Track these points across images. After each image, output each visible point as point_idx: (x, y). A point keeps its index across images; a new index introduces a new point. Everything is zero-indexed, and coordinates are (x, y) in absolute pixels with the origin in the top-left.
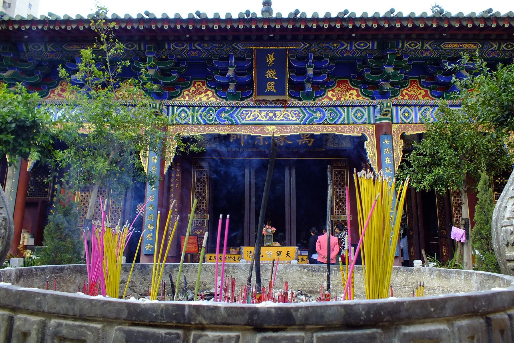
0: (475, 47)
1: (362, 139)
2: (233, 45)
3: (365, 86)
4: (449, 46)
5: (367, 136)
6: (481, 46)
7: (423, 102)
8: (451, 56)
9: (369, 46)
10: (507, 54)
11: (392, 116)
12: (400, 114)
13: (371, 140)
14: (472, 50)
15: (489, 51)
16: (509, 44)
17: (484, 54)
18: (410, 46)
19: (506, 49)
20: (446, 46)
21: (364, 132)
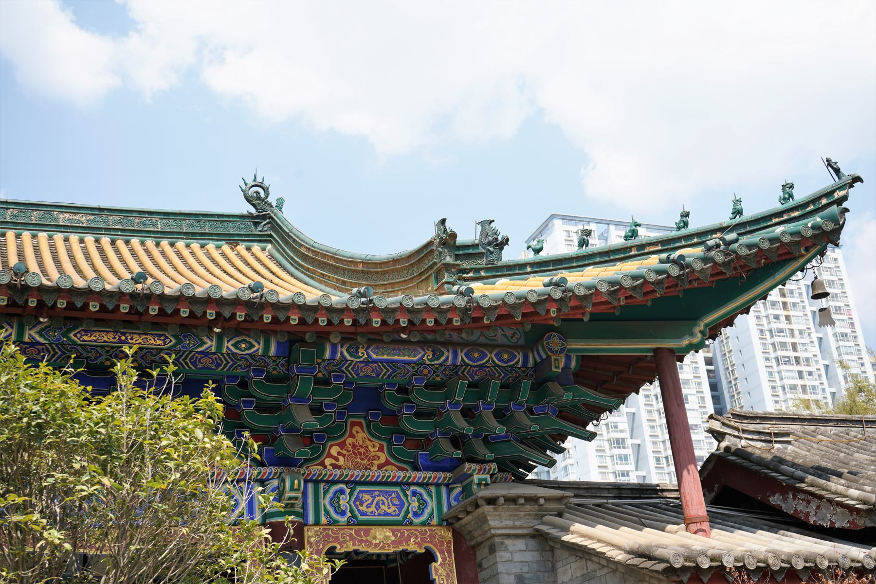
0: (159, 342)
1: (429, 557)
2: (71, 335)
3: (398, 440)
4: (93, 338)
5: (438, 554)
6: (174, 341)
7: (323, 473)
8: (98, 361)
9: (259, 348)
10: (240, 363)
11: (304, 506)
12: (325, 501)
13: (444, 559)
14: (152, 349)
15: (197, 352)
16: (241, 342)
17: (228, 362)
18: (236, 348)
19: (238, 351)
20: (85, 338)
21: (431, 543)
